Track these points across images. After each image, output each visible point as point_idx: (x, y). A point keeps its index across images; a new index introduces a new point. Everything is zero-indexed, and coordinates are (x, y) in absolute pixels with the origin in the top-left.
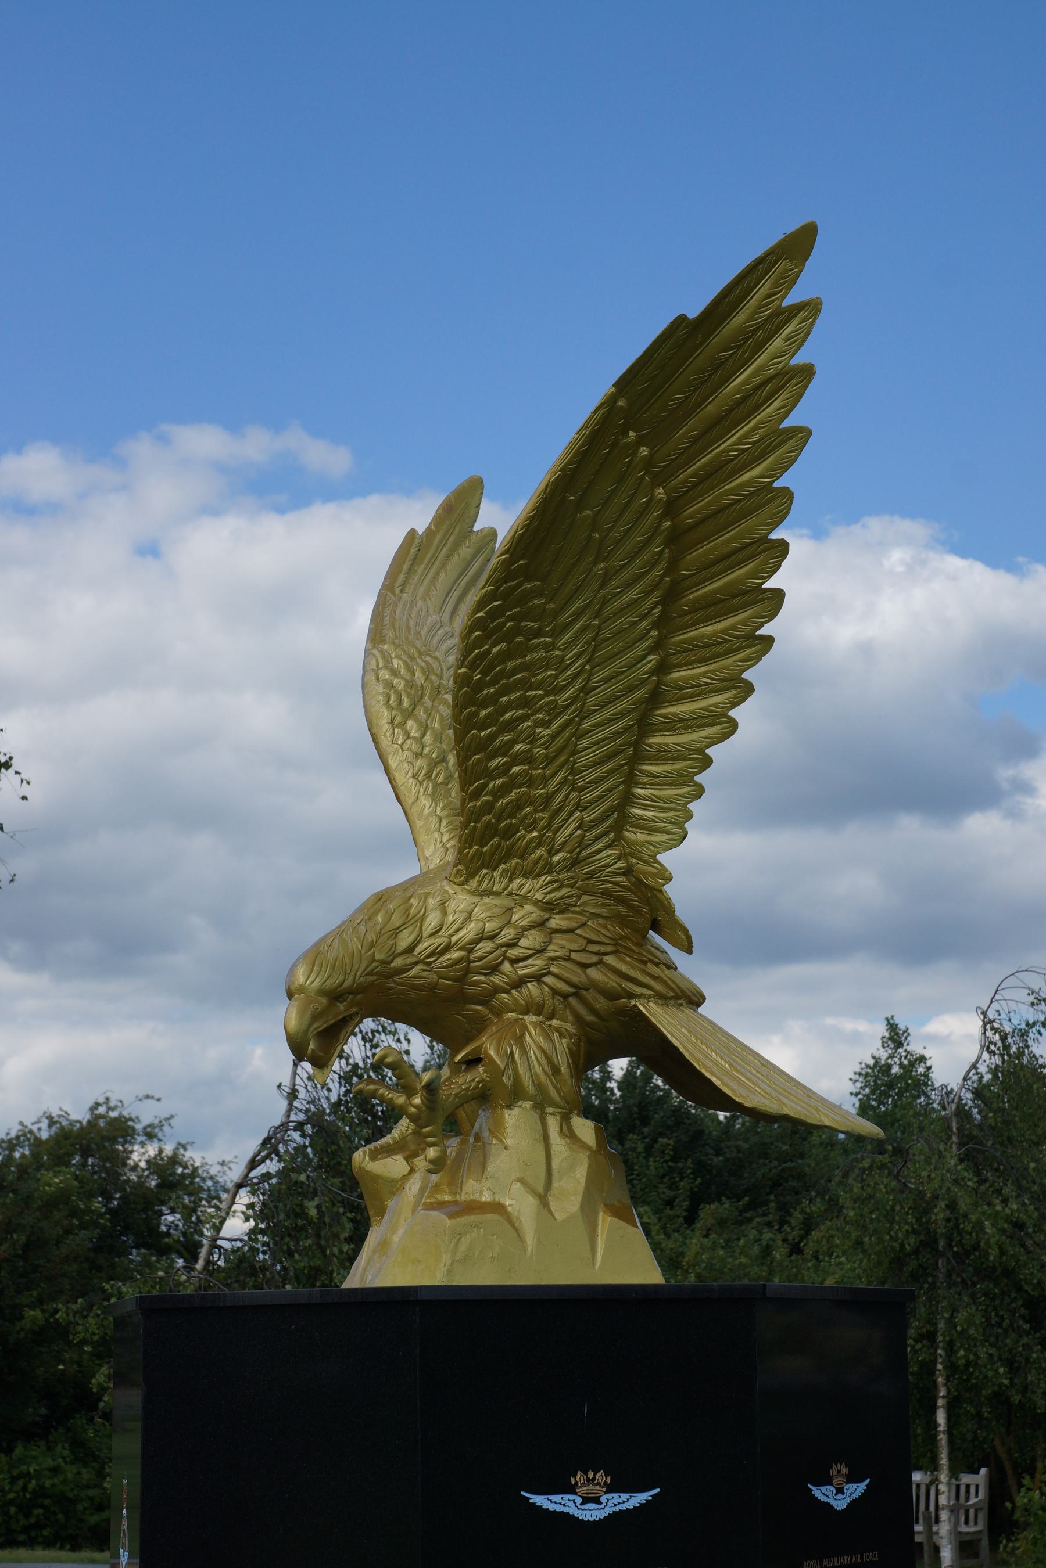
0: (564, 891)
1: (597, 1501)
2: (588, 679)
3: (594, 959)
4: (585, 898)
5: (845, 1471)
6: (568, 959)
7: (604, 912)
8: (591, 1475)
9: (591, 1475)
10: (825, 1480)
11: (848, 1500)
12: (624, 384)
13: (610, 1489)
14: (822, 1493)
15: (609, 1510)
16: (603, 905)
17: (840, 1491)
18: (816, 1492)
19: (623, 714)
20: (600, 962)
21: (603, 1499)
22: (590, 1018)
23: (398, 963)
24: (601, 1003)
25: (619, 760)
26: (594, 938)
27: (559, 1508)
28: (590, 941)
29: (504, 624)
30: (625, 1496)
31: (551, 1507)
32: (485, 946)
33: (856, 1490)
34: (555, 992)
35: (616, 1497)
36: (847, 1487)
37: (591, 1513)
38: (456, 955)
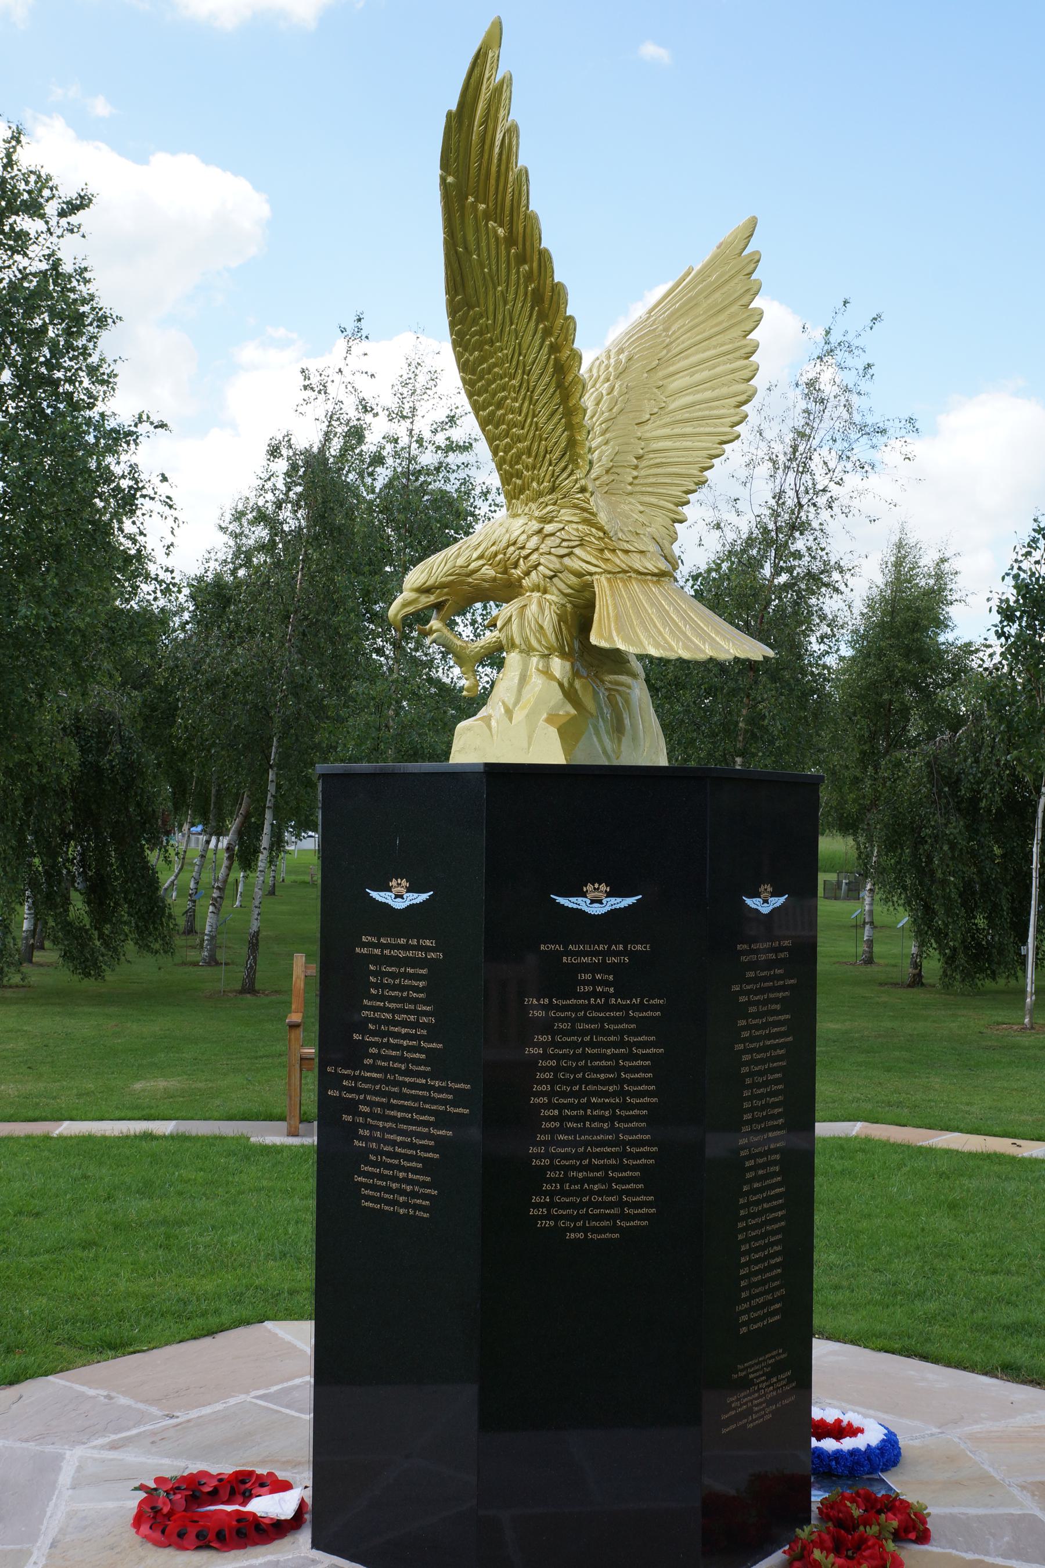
0: (549, 508)
1: (600, 902)
2: (524, 366)
3: (566, 551)
4: (563, 511)
5: (770, 889)
6: (550, 553)
7: (575, 519)
8: (596, 886)
9: (596, 886)
10: (756, 895)
11: (771, 908)
12: (445, 164)
13: (609, 895)
14: (752, 903)
15: (408, 903)
16: (575, 514)
17: (766, 901)
18: (749, 902)
19: (548, 385)
20: (571, 553)
21: (604, 901)
22: (570, 591)
23: (473, 566)
24: (573, 580)
25: (557, 417)
26: (567, 537)
27: (384, 900)
28: (564, 540)
29: (470, 340)
30: (619, 900)
31: (571, 905)
32: (512, 549)
33: (778, 901)
34: (545, 576)
35: (613, 900)
36: (770, 899)
37: (596, 910)
38: (500, 556)
